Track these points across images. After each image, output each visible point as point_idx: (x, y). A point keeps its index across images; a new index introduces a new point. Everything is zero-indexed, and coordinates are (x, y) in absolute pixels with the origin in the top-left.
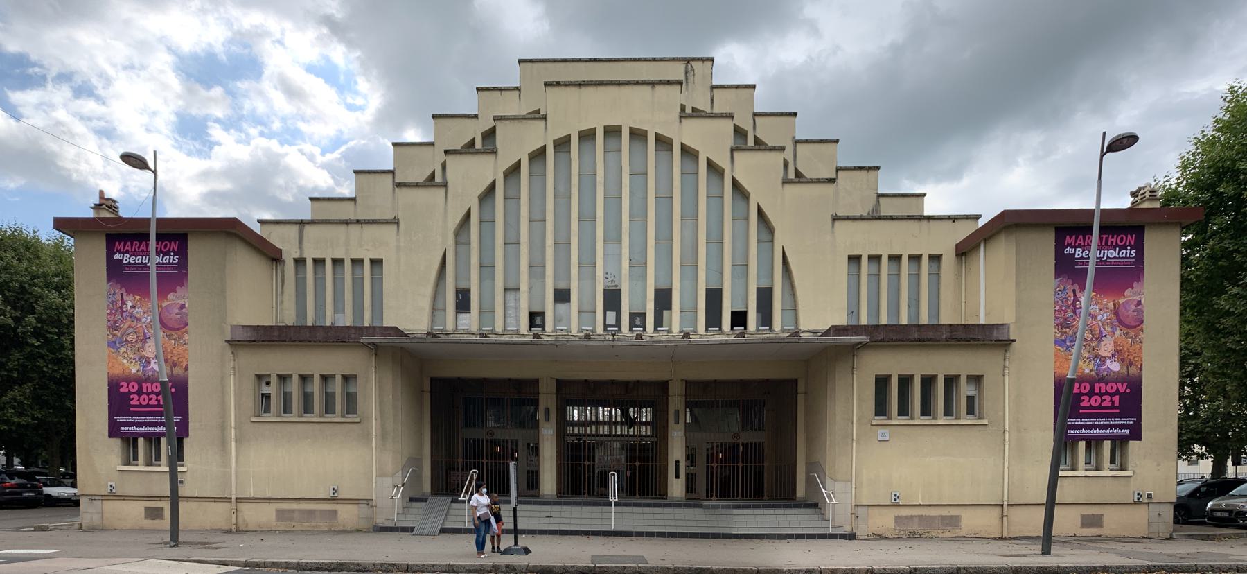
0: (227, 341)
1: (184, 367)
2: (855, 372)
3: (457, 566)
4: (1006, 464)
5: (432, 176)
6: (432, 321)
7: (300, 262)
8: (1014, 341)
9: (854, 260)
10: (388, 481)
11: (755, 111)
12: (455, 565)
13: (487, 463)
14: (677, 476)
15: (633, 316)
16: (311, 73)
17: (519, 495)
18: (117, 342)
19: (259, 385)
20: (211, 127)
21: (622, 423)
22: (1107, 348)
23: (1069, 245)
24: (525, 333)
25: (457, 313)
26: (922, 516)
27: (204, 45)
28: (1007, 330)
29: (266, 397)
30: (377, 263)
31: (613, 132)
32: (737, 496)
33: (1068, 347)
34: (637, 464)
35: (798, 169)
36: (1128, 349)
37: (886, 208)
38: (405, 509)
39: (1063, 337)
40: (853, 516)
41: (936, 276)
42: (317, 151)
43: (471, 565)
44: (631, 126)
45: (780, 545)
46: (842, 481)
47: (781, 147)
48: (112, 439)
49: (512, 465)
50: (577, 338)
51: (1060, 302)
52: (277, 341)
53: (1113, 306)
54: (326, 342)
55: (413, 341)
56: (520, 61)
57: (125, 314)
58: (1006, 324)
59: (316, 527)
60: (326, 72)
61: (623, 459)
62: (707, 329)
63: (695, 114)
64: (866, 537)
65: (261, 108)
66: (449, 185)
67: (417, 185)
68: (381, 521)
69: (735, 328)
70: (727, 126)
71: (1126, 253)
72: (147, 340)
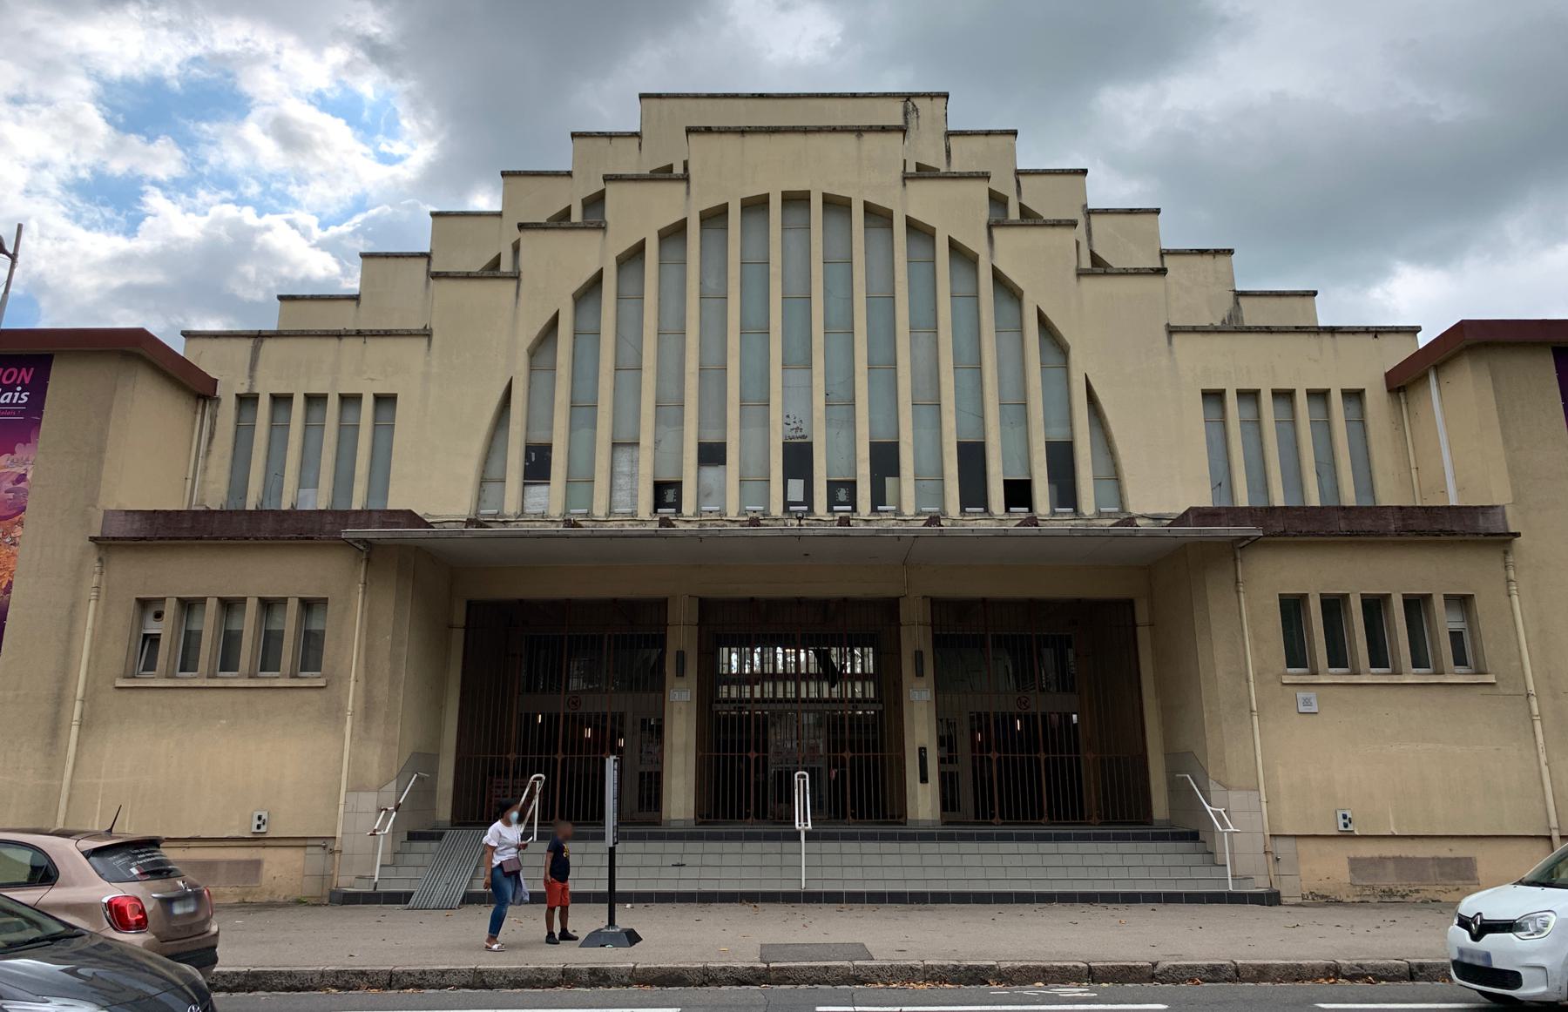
0: (92, 539)
2: (1241, 589)
3: (490, 972)
4: (1543, 758)
5: (496, 263)
6: (479, 499)
7: (247, 401)
8: (1517, 535)
9: (1214, 397)
10: (369, 801)
11: (1018, 168)
12: (487, 970)
13: (564, 761)
14: (924, 779)
15: (832, 486)
16: (327, 112)
17: (621, 820)
19: (141, 622)
20: (146, 192)
21: (818, 678)
24: (647, 517)
25: (525, 484)
26: (1400, 857)
27: (147, 68)
28: (1501, 517)
29: (153, 640)
30: (385, 401)
31: (796, 200)
32: (1041, 817)
34: (847, 755)
35: (1096, 252)
37: (1253, 314)
38: (399, 857)
40: (1270, 856)
41: (1359, 423)
42: (313, 222)
43: (520, 971)
44: (825, 191)
45: (1127, 913)
46: (1240, 789)
47: (1071, 221)
49: (611, 763)
50: (738, 524)
52: (185, 538)
54: (278, 538)
55: (440, 535)
56: (642, 96)
58: (1497, 506)
60: (345, 108)
61: (821, 745)
62: (962, 510)
63: (920, 173)
64: (1300, 900)
65: (236, 159)
66: (523, 276)
67: (468, 276)
68: (347, 881)
69: (1012, 509)
70: (980, 190)
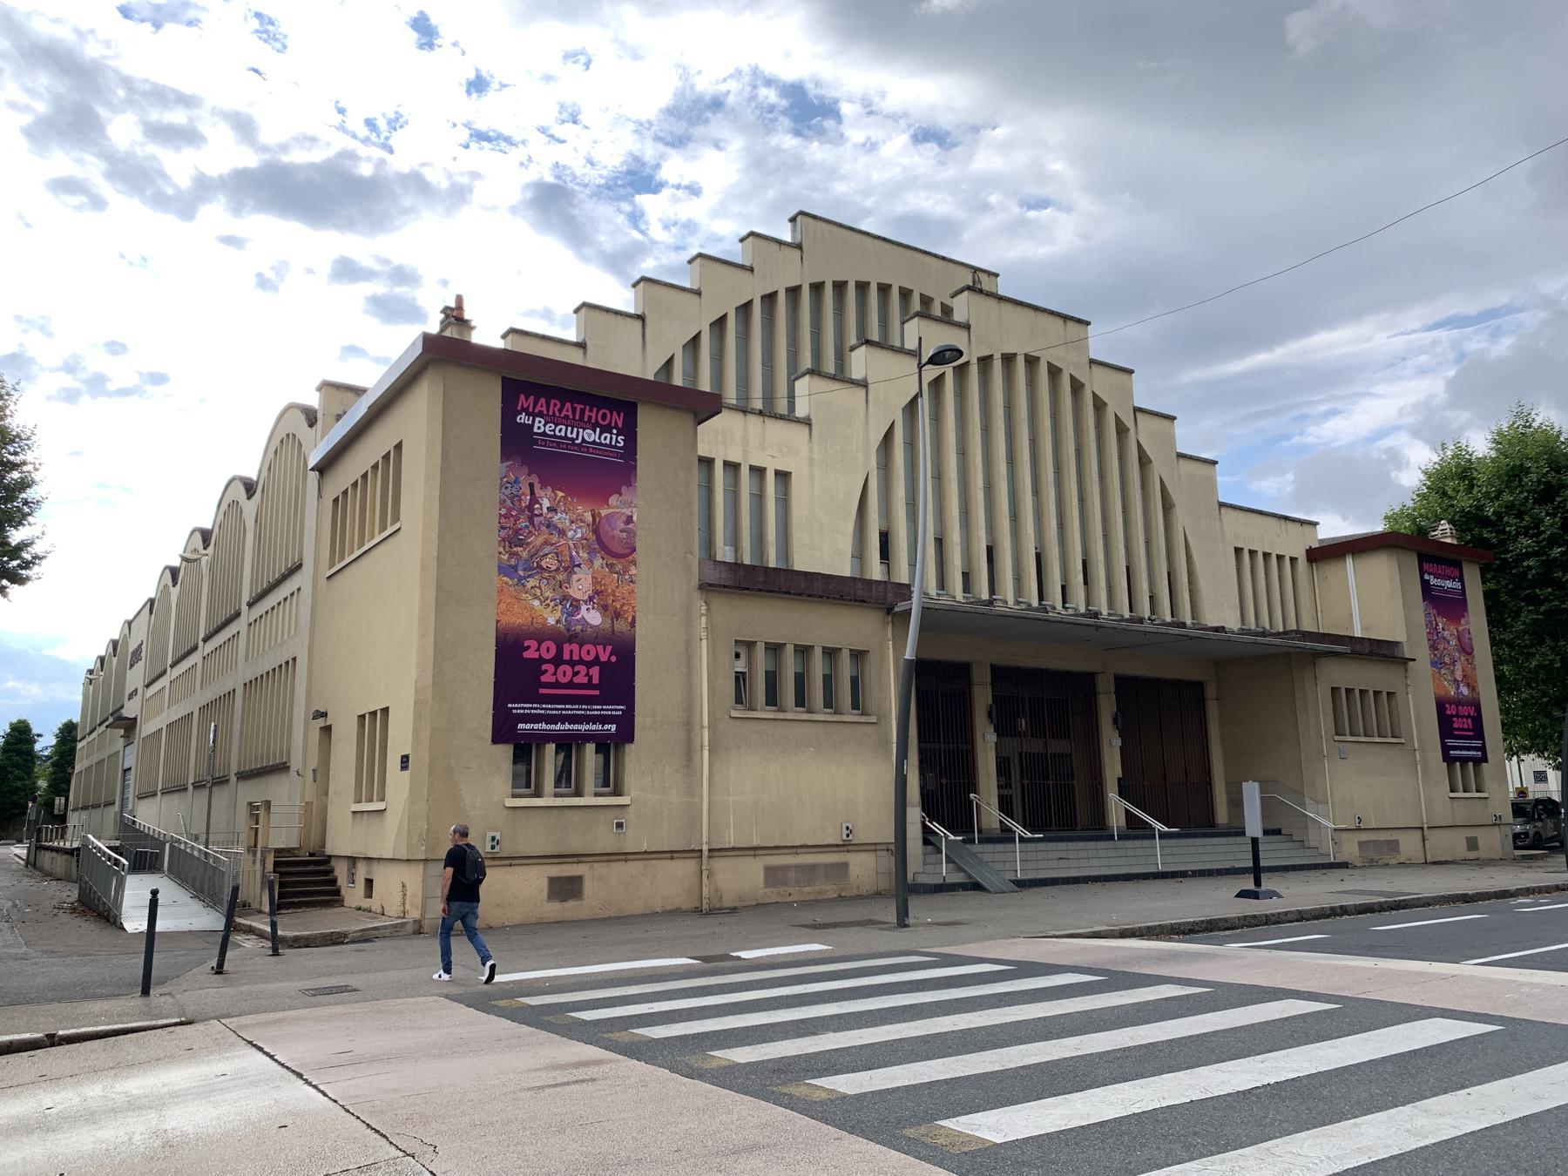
1: (630, 620)
9: (1238, 551)
18: (520, 568)
22: (581, 585)
23: (525, 410)
33: (520, 579)
36: (614, 591)
39: (513, 562)
48: (494, 746)
51: (509, 502)
53: (591, 519)
57: (537, 520)
59: (820, 893)
71: (611, 438)
72: (576, 569)
